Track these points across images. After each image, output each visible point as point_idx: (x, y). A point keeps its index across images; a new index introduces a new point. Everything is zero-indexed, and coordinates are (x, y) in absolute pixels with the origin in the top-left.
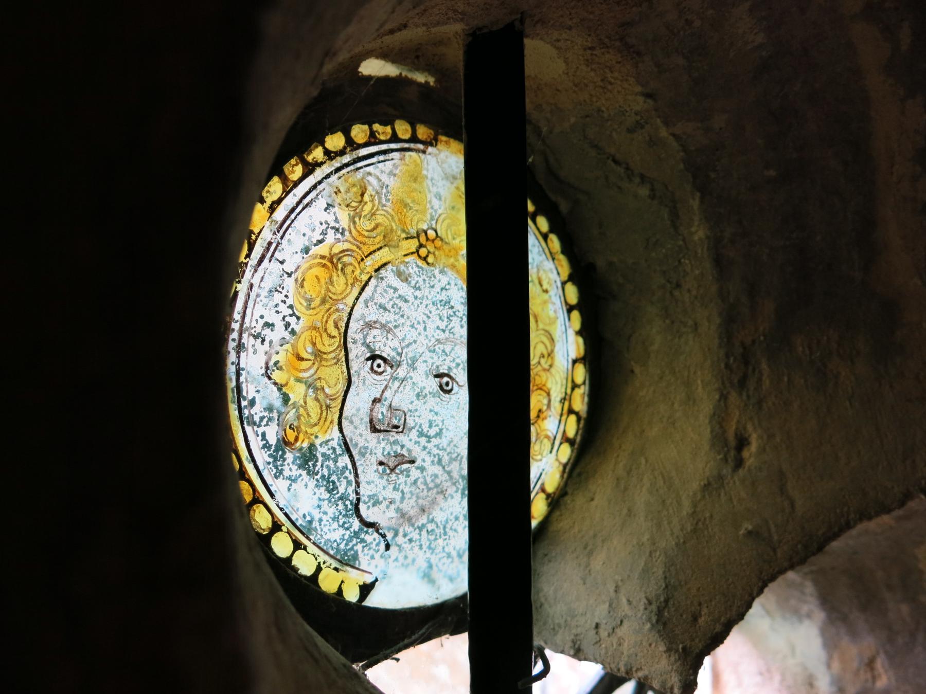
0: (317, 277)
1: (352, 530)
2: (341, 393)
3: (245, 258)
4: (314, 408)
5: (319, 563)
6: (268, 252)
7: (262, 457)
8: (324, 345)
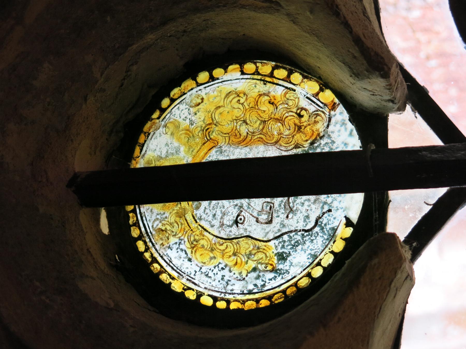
0: (201, 255)
1: (319, 231)
2: (252, 241)
3: (194, 291)
4: (260, 255)
5: (329, 252)
6: (191, 281)
7: (279, 281)
8: (230, 251)
